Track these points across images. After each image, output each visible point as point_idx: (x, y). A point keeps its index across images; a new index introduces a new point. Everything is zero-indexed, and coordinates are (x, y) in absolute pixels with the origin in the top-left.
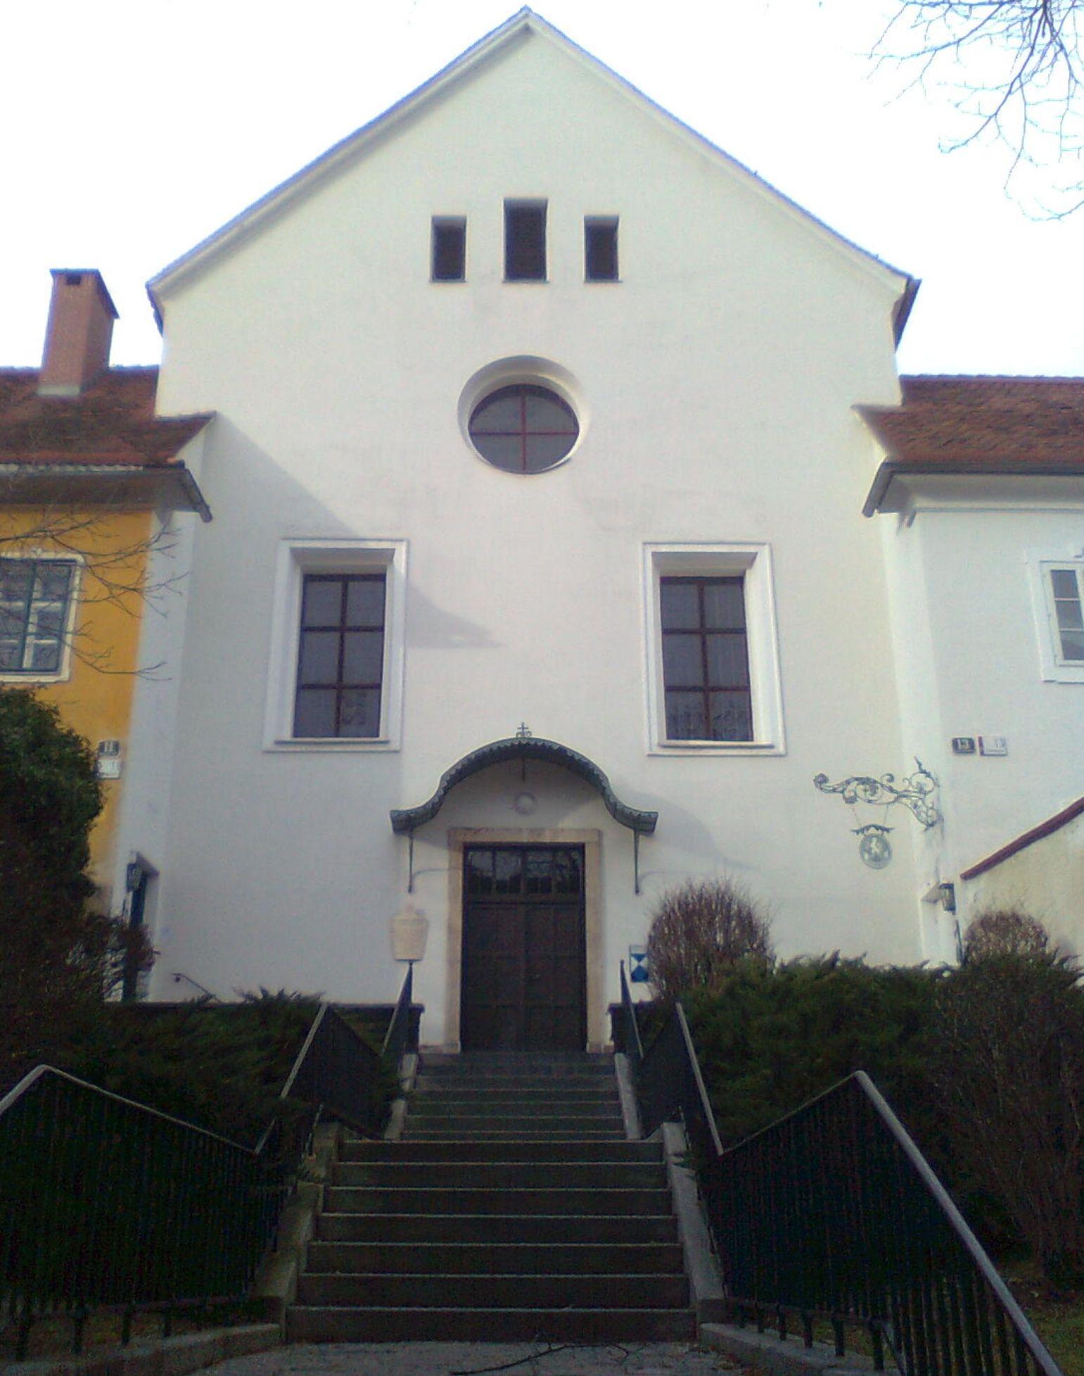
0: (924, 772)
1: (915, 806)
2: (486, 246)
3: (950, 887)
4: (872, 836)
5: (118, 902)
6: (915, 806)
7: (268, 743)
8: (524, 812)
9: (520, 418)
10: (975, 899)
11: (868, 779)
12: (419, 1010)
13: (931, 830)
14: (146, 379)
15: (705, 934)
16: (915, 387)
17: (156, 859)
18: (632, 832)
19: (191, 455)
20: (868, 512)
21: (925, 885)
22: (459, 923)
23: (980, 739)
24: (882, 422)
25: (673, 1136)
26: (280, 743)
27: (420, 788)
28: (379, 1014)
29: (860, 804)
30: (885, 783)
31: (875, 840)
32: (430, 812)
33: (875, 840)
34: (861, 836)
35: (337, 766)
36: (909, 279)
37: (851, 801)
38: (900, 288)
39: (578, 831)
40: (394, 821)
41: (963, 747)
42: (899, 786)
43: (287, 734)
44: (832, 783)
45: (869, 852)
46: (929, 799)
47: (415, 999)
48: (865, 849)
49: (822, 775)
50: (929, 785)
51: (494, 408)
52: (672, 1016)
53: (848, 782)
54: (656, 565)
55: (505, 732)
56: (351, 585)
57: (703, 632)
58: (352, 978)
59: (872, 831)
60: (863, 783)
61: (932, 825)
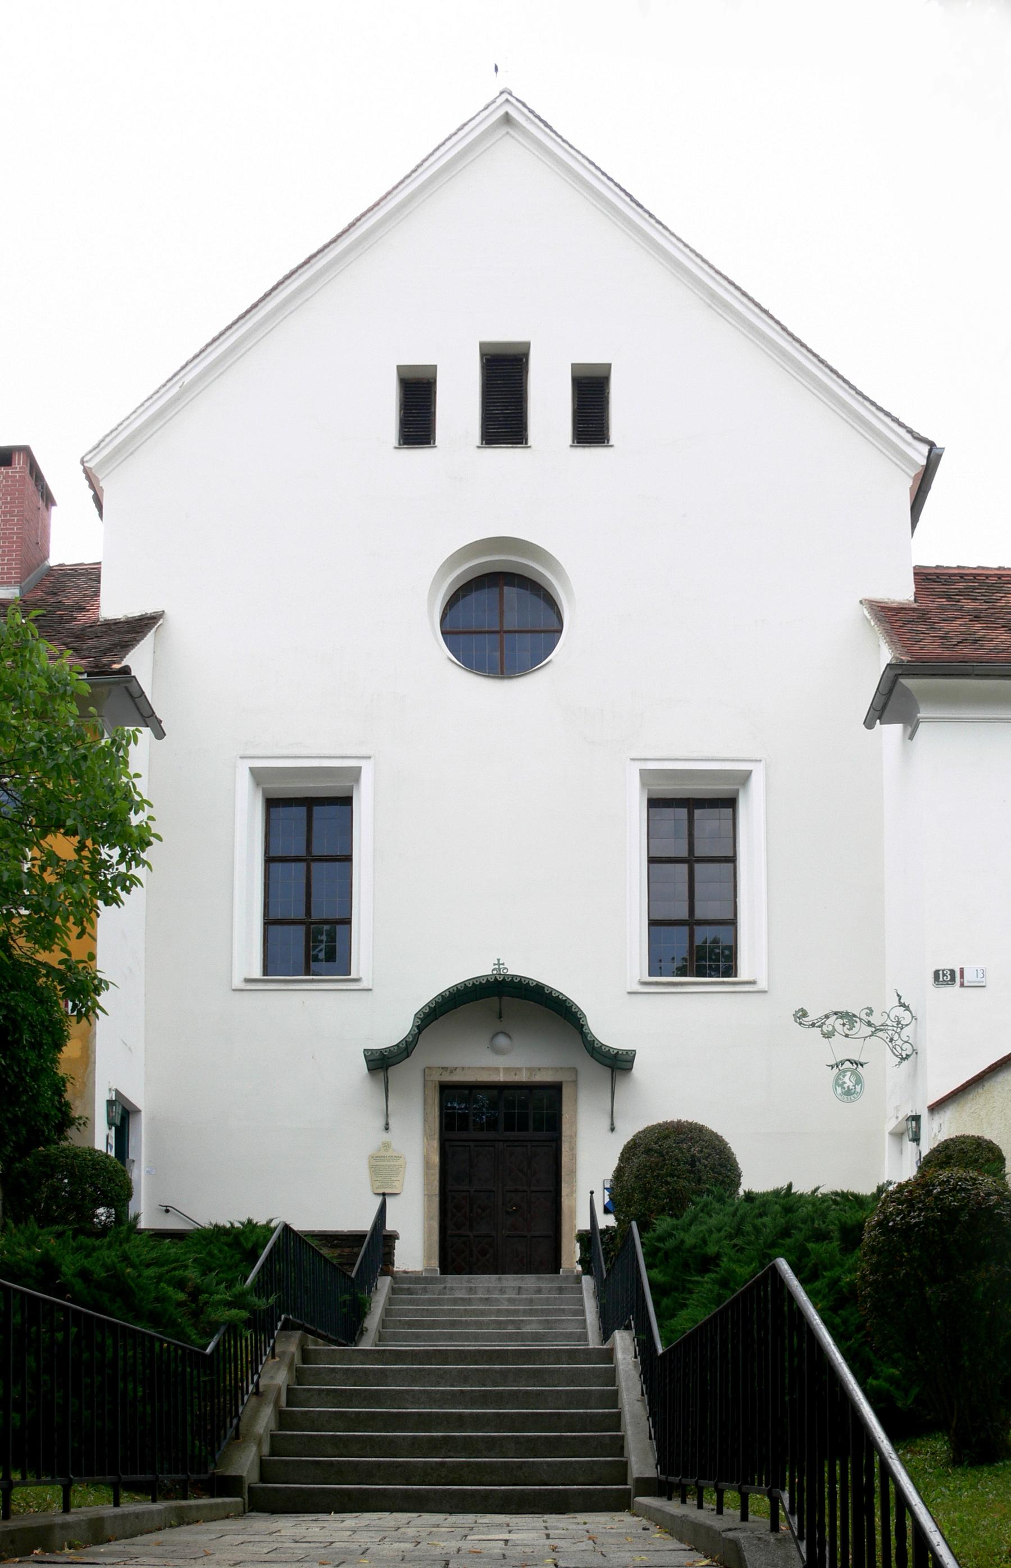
0: (903, 1005)
1: (891, 1040)
2: (459, 403)
3: (916, 1118)
4: (845, 1071)
5: (101, 1138)
6: (891, 1040)
7: (238, 983)
8: (498, 1051)
9: (500, 612)
10: (937, 1132)
11: (847, 1013)
12: (393, 1237)
13: (905, 1063)
14: (89, 576)
15: (677, 1166)
16: (927, 579)
17: (136, 1097)
18: (609, 1070)
19: (139, 661)
20: (869, 724)
21: (894, 1119)
22: (436, 1159)
23: (962, 971)
24: (889, 617)
25: (623, 1342)
26: (248, 981)
27: (393, 1029)
28: (354, 1239)
29: (837, 1038)
30: (863, 1016)
31: (849, 1074)
32: (404, 1050)
33: (849, 1074)
34: (836, 1070)
35: (310, 1007)
36: (932, 445)
37: (828, 1035)
38: (920, 455)
39: (556, 1070)
40: (368, 1061)
41: (945, 978)
42: (877, 1020)
43: (257, 972)
44: (812, 1016)
45: (842, 1086)
46: (906, 1032)
47: (390, 1226)
48: (838, 1082)
49: (802, 1010)
50: (906, 1018)
51: (473, 597)
52: (628, 1236)
53: (827, 1017)
54: (643, 784)
55: (481, 968)
56: (316, 810)
57: (691, 860)
58: (330, 1204)
59: (847, 1065)
60: (841, 1018)
61: (903, 1059)
